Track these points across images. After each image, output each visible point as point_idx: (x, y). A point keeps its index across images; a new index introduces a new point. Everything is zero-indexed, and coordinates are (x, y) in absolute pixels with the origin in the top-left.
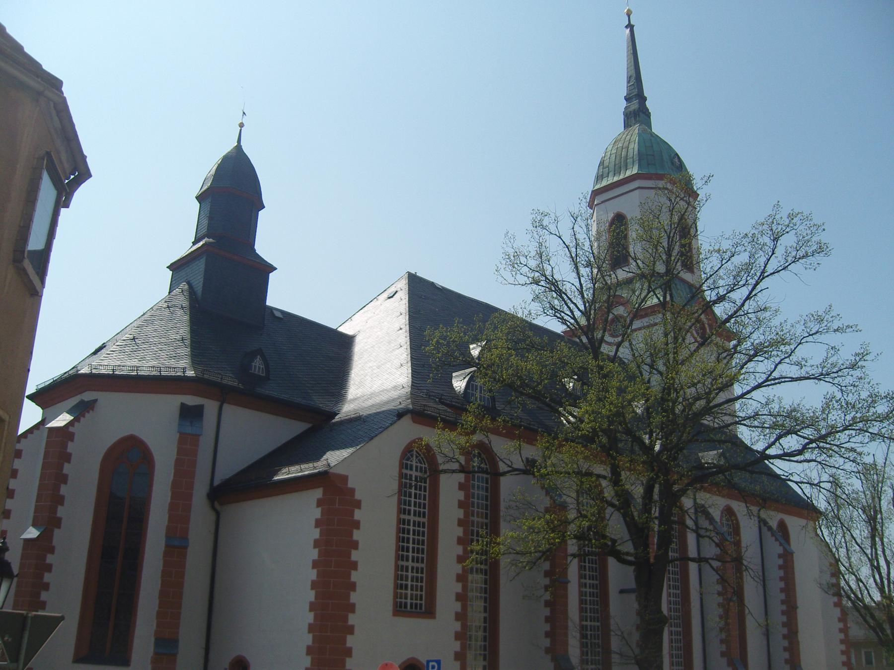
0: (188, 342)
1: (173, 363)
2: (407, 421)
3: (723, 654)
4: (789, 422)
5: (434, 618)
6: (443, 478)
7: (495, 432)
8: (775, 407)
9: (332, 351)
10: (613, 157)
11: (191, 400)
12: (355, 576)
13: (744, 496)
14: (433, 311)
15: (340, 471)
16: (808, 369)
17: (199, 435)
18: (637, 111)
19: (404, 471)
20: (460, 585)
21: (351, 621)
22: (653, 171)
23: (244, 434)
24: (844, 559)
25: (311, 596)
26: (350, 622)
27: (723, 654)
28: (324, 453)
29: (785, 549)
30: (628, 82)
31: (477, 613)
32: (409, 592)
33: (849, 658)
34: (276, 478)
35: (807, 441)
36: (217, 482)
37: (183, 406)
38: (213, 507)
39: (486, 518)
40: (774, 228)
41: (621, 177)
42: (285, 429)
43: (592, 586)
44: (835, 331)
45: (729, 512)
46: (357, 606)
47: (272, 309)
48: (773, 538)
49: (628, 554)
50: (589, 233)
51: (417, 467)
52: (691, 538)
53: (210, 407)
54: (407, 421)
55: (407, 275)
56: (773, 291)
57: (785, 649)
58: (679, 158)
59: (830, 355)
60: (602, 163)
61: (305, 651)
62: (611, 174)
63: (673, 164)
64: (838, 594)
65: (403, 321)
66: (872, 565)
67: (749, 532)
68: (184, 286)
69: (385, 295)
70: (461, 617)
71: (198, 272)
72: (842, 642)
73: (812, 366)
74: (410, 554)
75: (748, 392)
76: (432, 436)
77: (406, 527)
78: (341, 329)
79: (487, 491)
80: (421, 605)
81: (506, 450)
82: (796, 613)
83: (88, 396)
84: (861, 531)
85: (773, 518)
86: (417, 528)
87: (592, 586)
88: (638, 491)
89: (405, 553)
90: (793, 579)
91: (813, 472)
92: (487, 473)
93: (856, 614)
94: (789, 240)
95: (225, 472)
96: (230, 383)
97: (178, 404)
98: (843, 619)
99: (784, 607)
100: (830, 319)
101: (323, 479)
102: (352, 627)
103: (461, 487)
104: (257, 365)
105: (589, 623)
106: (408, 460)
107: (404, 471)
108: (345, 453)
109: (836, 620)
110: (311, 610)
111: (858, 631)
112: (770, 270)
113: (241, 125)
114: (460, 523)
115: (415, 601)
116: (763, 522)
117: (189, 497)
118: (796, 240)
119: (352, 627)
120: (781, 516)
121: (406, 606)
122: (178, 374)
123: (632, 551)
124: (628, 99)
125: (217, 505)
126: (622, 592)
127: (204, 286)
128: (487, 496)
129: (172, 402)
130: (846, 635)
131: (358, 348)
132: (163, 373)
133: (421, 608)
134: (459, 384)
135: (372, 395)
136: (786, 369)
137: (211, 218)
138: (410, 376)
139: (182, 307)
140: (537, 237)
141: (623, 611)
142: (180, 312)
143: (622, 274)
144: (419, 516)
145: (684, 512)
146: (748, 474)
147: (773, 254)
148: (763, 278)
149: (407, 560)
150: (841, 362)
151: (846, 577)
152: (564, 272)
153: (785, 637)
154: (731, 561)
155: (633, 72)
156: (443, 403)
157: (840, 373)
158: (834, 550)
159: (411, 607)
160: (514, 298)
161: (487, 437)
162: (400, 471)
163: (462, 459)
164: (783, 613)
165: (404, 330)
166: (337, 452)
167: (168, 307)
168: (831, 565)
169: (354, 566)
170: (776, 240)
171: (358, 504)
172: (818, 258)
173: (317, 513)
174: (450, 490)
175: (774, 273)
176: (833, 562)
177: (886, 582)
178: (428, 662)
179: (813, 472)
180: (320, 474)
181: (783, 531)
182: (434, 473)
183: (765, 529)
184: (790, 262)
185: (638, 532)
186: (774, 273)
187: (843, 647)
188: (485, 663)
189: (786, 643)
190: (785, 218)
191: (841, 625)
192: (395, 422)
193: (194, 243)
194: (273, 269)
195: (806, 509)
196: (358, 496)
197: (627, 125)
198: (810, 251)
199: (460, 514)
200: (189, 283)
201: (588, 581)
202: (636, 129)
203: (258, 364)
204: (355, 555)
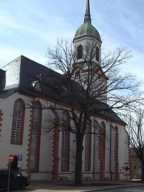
3: (99, 158)
13: (107, 119)
18: (88, 18)
19: (13, 130)
24: (131, 136)
31: (34, 145)
32: (15, 138)
33: (130, 160)
45: (103, 123)
50: (72, 48)
52: (93, 128)
54: (17, 93)
63: (96, 33)
66: (138, 137)
67: (108, 127)
70: (29, 145)
74: (16, 133)
76: (24, 97)
79: (39, 113)
84: (136, 129)
85: (114, 125)
86: (18, 124)
88: (78, 115)
92: (39, 109)
106: (17, 103)
111: (134, 153)
121: (14, 142)
123: (75, 130)
126: (73, 141)
133: (18, 142)
141: (73, 146)
143: (79, 61)
145: (90, 121)
146: (108, 114)
154: (103, 133)
156: (28, 90)
159: (16, 142)
163: (31, 104)
168: (128, 137)
174: (28, 113)
176: (128, 136)
177: (140, 142)
178: (19, 156)
185: (77, 125)
192: (14, 93)
199: (31, 118)
202: (87, 23)
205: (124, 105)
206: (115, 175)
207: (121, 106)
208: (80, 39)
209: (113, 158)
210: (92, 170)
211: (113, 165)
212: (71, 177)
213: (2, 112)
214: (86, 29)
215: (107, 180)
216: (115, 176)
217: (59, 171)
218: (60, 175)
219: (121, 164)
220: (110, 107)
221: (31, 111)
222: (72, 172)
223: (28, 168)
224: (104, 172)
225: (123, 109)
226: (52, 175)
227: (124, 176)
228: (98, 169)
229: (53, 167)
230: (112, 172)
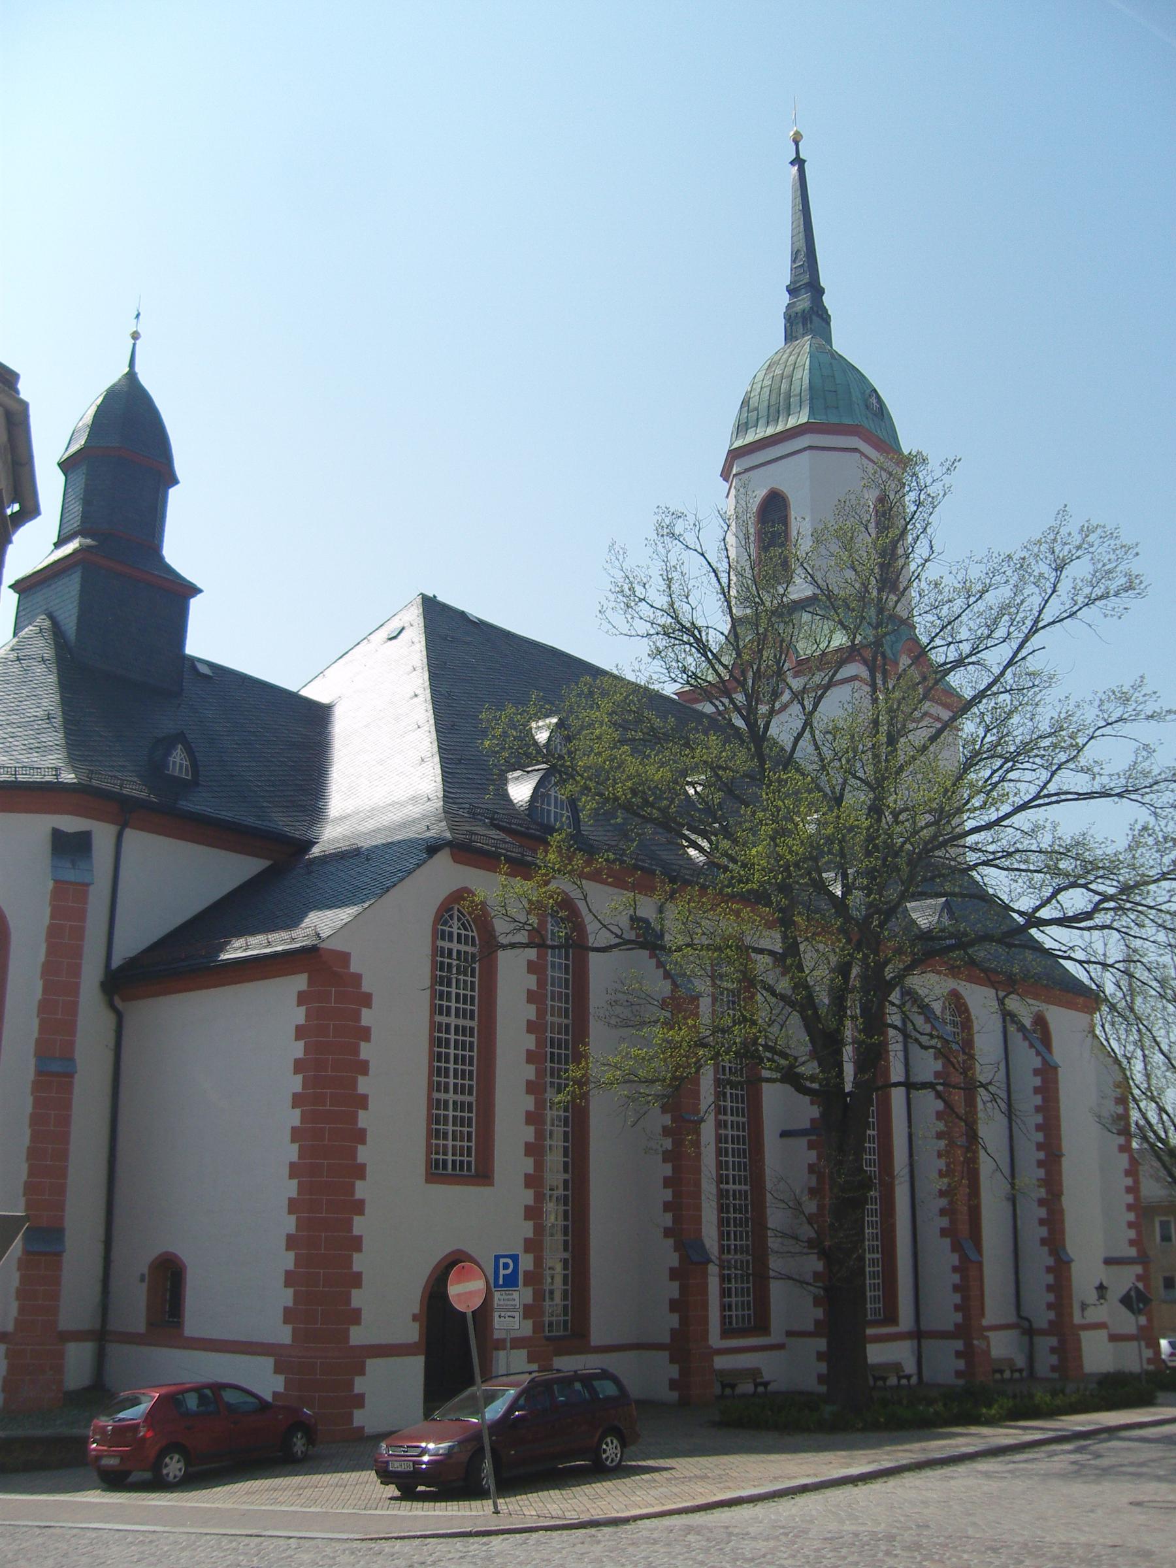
0: (58, 722)
1: (34, 759)
2: (443, 859)
3: (944, 1232)
4: (1072, 866)
5: (491, 1184)
6: (502, 956)
7: (595, 877)
8: (1045, 841)
9: (295, 733)
10: (766, 391)
11: (70, 824)
12: (364, 1119)
13: (1006, 983)
14: (480, 672)
15: (337, 945)
16: (1105, 780)
17: (88, 885)
18: (808, 313)
19: (440, 943)
20: (531, 1129)
22: (833, 420)
23: (162, 880)
24: (1139, 1077)
25: (292, 1152)
26: (359, 1195)
27: (944, 1232)
28: (305, 915)
29: (1044, 1061)
30: (794, 261)
34: (224, 956)
35: (1098, 898)
36: (116, 962)
37: (57, 835)
38: (112, 1006)
39: (566, 1017)
40: (1057, 550)
41: (780, 428)
42: (230, 870)
43: (737, 1126)
44: (1149, 717)
46: (368, 1169)
47: (193, 660)
48: (1027, 1043)
49: (812, 1078)
51: (459, 935)
52: (895, 1047)
53: (103, 834)
54: (443, 859)
55: (419, 600)
56: (1051, 651)
57: (1042, 1222)
58: (878, 397)
59: (1140, 759)
60: (746, 403)
61: (283, 1243)
62: (762, 422)
63: (867, 407)
64: (1125, 1132)
65: (420, 681)
68: (42, 621)
69: (383, 633)
71: (67, 599)
72: (1130, 1207)
73: (1110, 775)
75: (1007, 816)
76: (493, 889)
77: (444, 1035)
78: (303, 693)
80: (469, 1163)
81: (607, 907)
82: (1060, 1164)
85: (1024, 1009)
87: (737, 1126)
89: (443, 1080)
90: (1058, 1110)
91: (1112, 947)
93: (1157, 1164)
94: (1079, 570)
95: (129, 945)
96: (136, 793)
97: (49, 830)
98: (1132, 1171)
99: (1041, 1155)
100: (1141, 699)
101: (308, 958)
103: (532, 967)
104: (178, 760)
105: (731, 1187)
106: (445, 923)
107: (440, 943)
108: (344, 915)
110: (291, 1177)
111: (1153, 1189)
112: (1047, 617)
113: (135, 336)
115: (459, 1158)
116: (1008, 1016)
117: (73, 989)
118: (1091, 568)
120: (1037, 1006)
121: (445, 1167)
122: (48, 779)
124: (792, 291)
126: (784, 1134)
127: (80, 618)
128: (567, 980)
129: (36, 828)
130: (1137, 1198)
131: (341, 728)
132: (21, 778)
133: (469, 1169)
134: (520, 791)
135: (373, 812)
136: (1069, 780)
137: (87, 502)
138: (439, 779)
139: (43, 660)
140: (663, 551)
142: (39, 669)
144: (464, 1017)
146: (1001, 949)
147: (1054, 591)
148: (1036, 631)
149: (446, 1091)
150: (1155, 772)
151: (1142, 1105)
153: (1041, 1202)
154: (958, 1085)
155: (802, 244)
157: (1155, 787)
158: (1124, 1062)
159: (454, 1168)
160: (628, 654)
161: (580, 887)
162: (434, 942)
164: (1040, 1164)
165: (421, 698)
166: (329, 913)
167: (18, 659)
170: (1059, 569)
171: (366, 1000)
172: (1126, 599)
173: (299, 1016)
174: (513, 975)
175: (1053, 622)
179: (1112, 947)
180: (303, 950)
181: (1041, 1034)
182: (490, 945)
183: (1012, 1029)
184: (1080, 604)
185: (827, 1044)
186: (1053, 622)
187: (1131, 1216)
188: (567, 1255)
189: (1043, 1213)
190: (1075, 533)
191: (1129, 1181)
192: (425, 862)
193: (57, 545)
194: (195, 591)
195: (1086, 998)
196: (366, 987)
197: (790, 337)
198: (1113, 586)
199: (531, 1012)
200: (51, 617)
201: (729, 1118)
202: (805, 344)
203: (178, 759)
204: (364, 1085)
205: (1101, 902)
206: (1053, 1341)
207: (1089, 908)
208: (768, 451)
209: (1034, 1232)
210: (906, 1320)
211: (1037, 1279)
212: (787, 1362)
213: (1046, 1248)
214: (806, 382)
215: (1007, 1375)
216: (1053, 1350)
217: (715, 1339)
218: (720, 1362)
219: (1087, 1271)
220: (1021, 920)
221: (530, 962)
222: (789, 1334)
223: (537, 1327)
224: (985, 1322)
225: (1095, 928)
226: (672, 1360)
227: (1111, 1345)
228: (943, 1311)
229: (672, 1310)
230: (1035, 1326)
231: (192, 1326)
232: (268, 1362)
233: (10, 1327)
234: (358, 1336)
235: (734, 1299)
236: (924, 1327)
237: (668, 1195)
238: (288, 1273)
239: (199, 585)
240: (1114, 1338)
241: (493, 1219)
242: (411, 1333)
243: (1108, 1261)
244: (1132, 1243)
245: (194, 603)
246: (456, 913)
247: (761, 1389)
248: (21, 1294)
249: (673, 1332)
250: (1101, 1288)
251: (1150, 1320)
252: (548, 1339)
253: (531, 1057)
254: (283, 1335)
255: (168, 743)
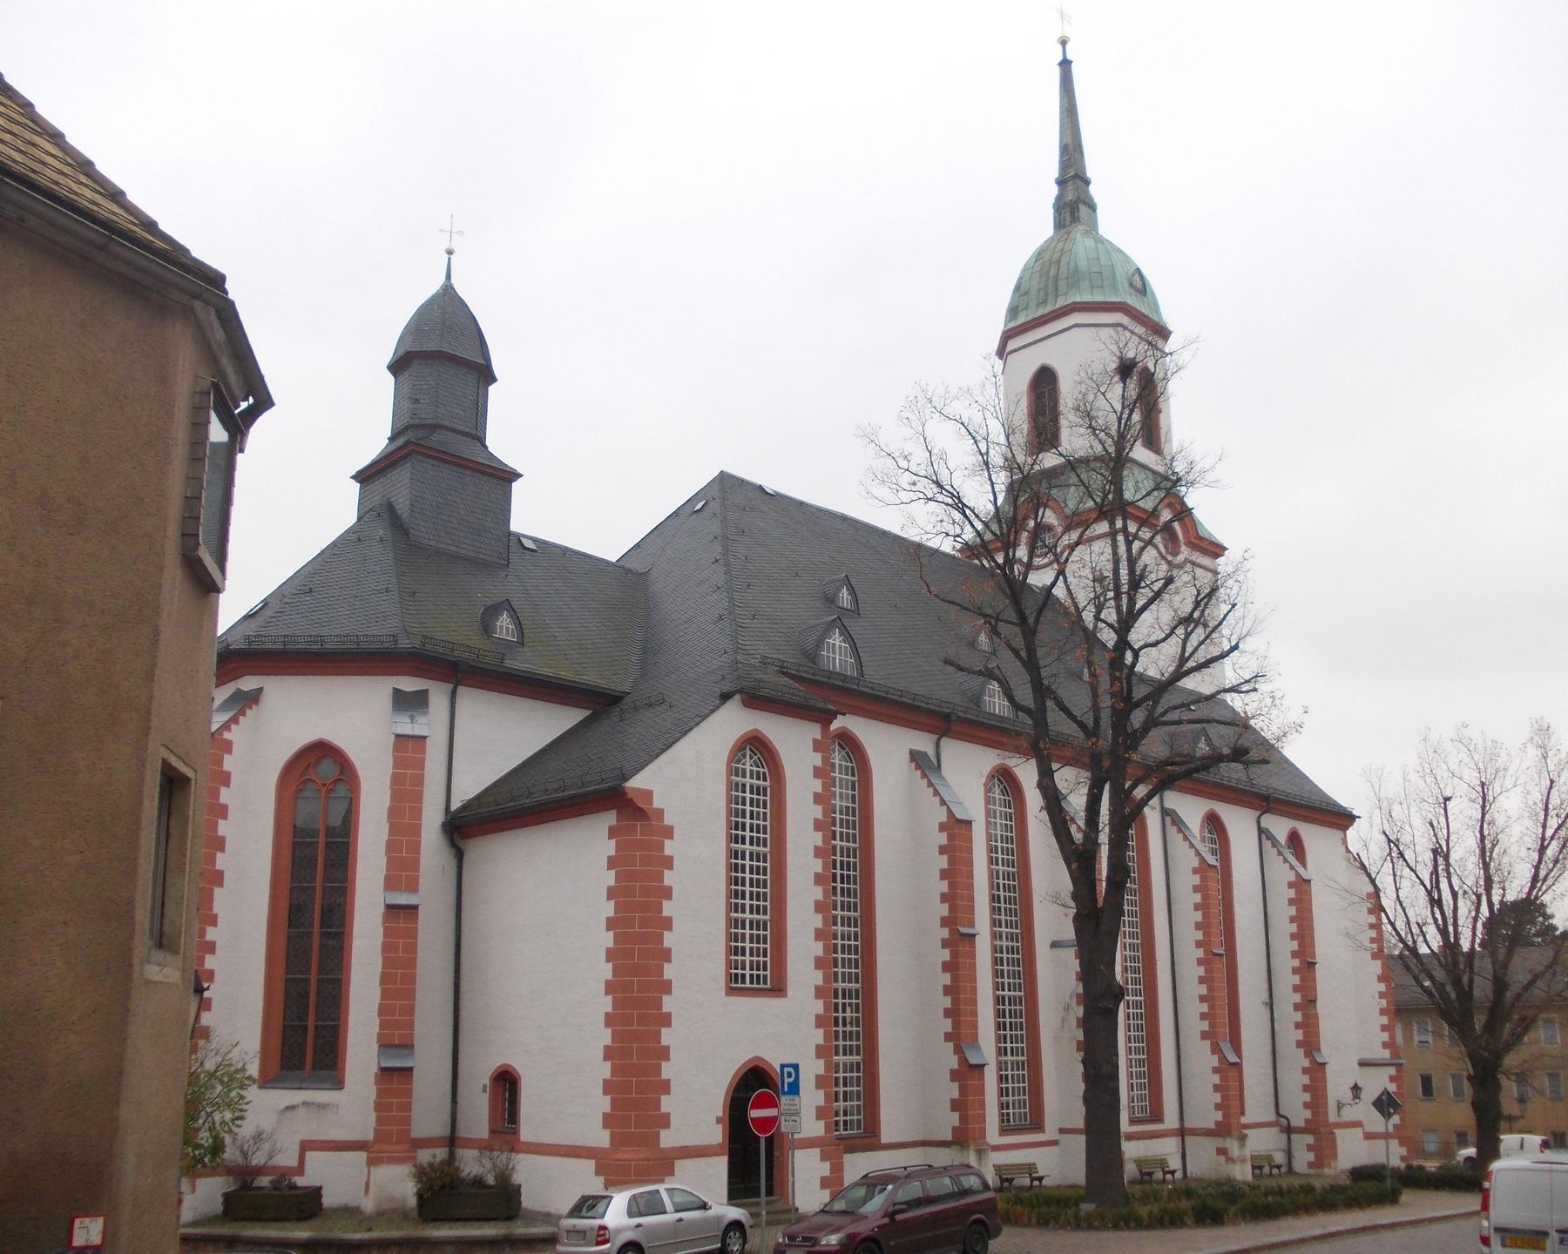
3: (1204, 1035)
11: (409, 684)
13: (1264, 802)
21: (666, 912)
27: (1204, 1035)
32: (748, 958)
33: (1392, 1037)
37: (397, 692)
43: (1011, 937)
83: (248, 683)
85: (1280, 827)
87: (1011, 937)
99: (1296, 962)
102: (669, 1015)
105: (1006, 993)
109: (1375, 978)
114: (818, 852)
115: (755, 971)
116: (1261, 831)
119: (669, 1015)
121: (743, 982)
124: (1061, 182)
125: (456, 838)
149: (743, 911)
152: (959, 459)
153: (1297, 1007)
155: (1068, 140)
169: (667, 924)
171: (669, 832)
173: (610, 848)
178: (783, 1066)
193: (391, 439)
194: (516, 476)
196: (668, 820)
203: (504, 623)
204: (668, 909)
206: (1309, 1139)
209: (1290, 1036)
210: (1171, 1120)
217: (993, 1135)
222: (1062, 1131)
224: (1244, 1120)
227: (1365, 1144)
228: (1205, 1113)
231: (527, 1133)
232: (590, 1165)
233: (370, 1137)
234: (668, 1139)
235: (1011, 1099)
236: (1187, 1125)
237: (947, 1002)
238: (605, 1082)
239: (520, 471)
240: (1369, 1136)
241: (787, 1031)
242: (715, 1134)
243: (1363, 1064)
244: (1385, 1045)
245: (516, 486)
246: (748, 752)
247: (1036, 1183)
248: (379, 1106)
249: (954, 1129)
250: (1356, 1089)
251: (1402, 1119)
252: (840, 1138)
253: (818, 879)
254: (602, 1139)
255: (492, 612)
